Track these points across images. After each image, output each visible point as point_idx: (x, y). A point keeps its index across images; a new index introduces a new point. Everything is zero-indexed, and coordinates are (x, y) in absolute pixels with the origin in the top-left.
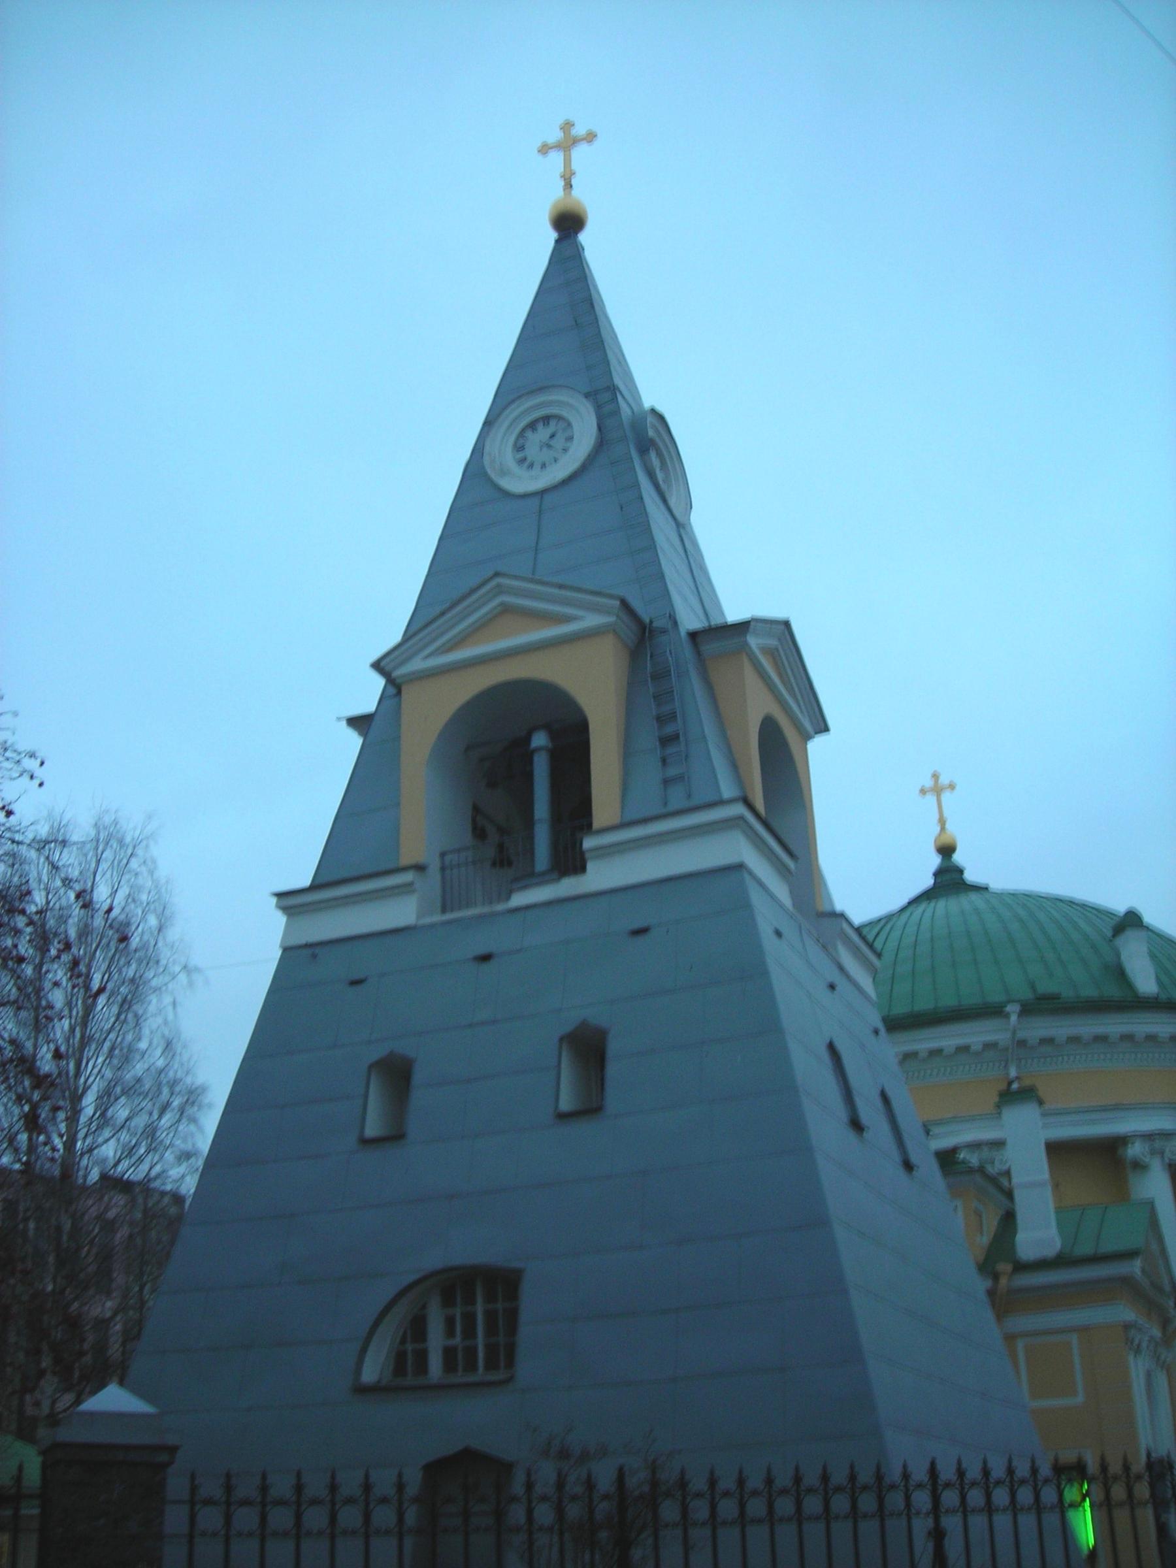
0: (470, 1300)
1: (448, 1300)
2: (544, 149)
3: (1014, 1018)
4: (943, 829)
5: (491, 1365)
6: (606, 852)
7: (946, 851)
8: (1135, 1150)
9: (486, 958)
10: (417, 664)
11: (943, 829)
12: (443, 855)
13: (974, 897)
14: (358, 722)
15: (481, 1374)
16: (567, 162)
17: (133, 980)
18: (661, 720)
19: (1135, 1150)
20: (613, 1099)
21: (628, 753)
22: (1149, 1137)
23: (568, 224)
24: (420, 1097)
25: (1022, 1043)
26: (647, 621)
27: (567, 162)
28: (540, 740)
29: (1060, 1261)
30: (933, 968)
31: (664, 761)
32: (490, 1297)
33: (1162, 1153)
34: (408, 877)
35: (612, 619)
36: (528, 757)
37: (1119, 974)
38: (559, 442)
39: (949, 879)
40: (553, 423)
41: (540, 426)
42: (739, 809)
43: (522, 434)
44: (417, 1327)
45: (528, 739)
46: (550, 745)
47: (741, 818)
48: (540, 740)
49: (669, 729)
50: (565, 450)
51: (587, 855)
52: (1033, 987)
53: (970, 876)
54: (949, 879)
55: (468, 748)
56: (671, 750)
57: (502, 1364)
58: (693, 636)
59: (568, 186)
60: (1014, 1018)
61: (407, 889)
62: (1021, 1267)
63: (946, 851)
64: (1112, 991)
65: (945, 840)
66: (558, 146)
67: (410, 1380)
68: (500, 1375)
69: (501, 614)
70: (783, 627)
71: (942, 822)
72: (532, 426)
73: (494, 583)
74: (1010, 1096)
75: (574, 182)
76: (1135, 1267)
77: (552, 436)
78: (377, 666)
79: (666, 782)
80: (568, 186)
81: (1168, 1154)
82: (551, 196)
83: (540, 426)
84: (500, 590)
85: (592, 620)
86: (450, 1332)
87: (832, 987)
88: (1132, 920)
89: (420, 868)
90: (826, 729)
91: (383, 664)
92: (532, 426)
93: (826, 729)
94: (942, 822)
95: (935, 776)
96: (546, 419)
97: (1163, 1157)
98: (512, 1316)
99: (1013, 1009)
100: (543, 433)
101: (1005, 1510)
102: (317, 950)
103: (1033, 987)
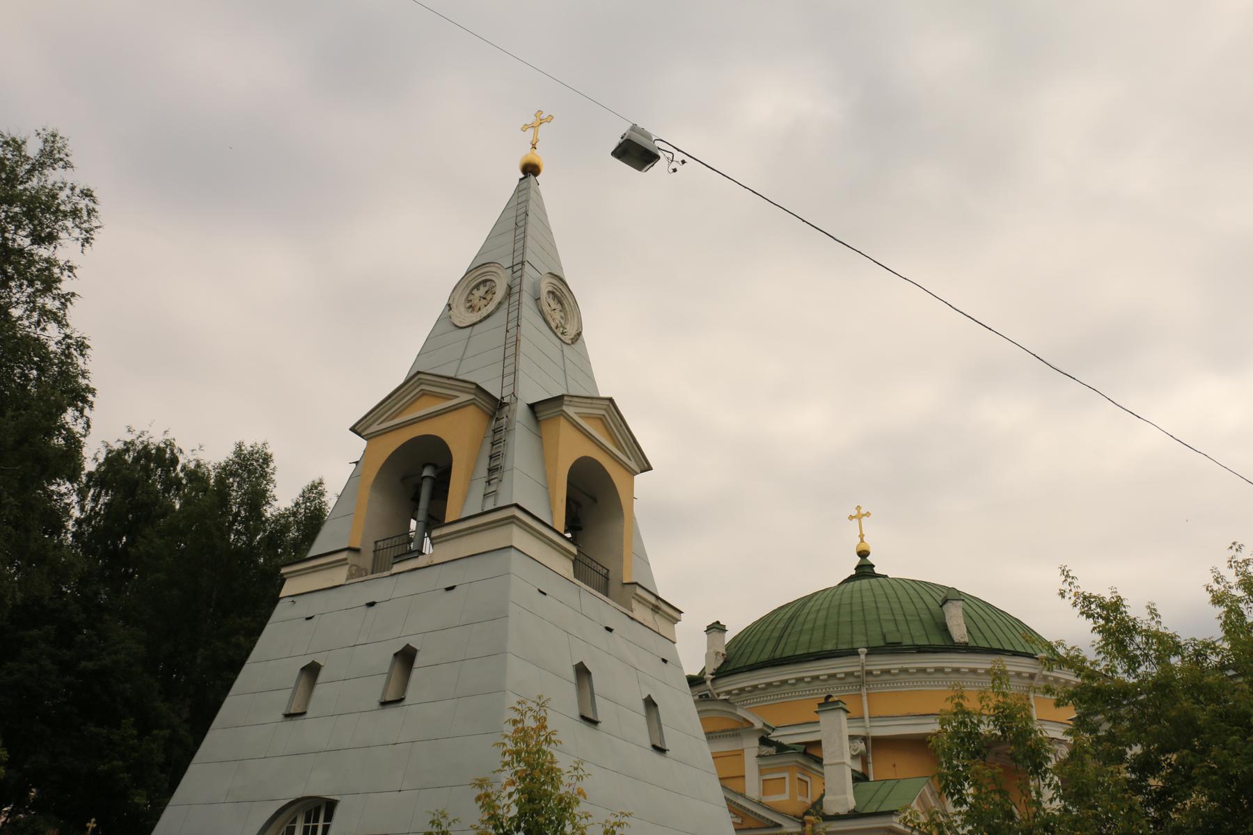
0: (316, 820)
3: (863, 657)
4: (862, 541)
7: (863, 554)
9: (371, 604)
11: (862, 541)
12: (376, 542)
16: (536, 134)
17: (1148, 637)
20: (410, 696)
21: (471, 480)
23: (531, 170)
24: (320, 690)
25: (869, 673)
27: (536, 134)
29: (854, 815)
30: (825, 625)
31: (489, 482)
35: (472, 397)
37: (944, 629)
39: (865, 570)
52: (884, 637)
53: (877, 570)
54: (865, 570)
55: (403, 479)
60: (863, 657)
62: (827, 818)
63: (863, 554)
64: (937, 640)
65: (863, 547)
71: (862, 536)
72: (477, 287)
74: (828, 704)
82: (523, 153)
83: (482, 287)
85: (464, 397)
92: (477, 287)
94: (862, 536)
95: (858, 508)
96: (485, 282)
99: (863, 650)
100: (483, 290)
103: (884, 637)
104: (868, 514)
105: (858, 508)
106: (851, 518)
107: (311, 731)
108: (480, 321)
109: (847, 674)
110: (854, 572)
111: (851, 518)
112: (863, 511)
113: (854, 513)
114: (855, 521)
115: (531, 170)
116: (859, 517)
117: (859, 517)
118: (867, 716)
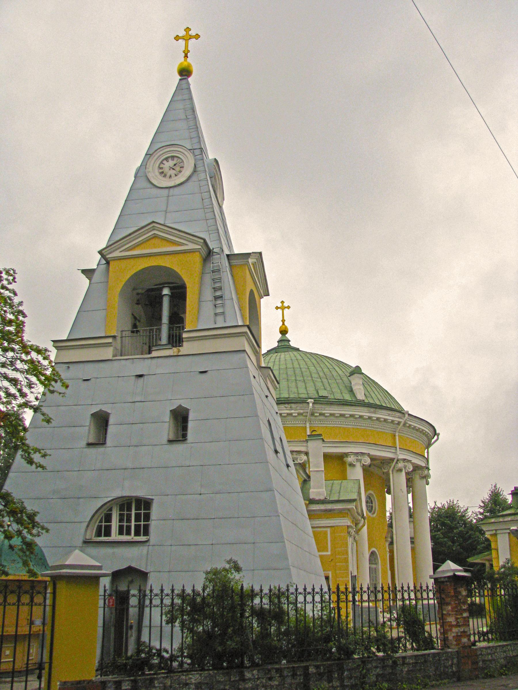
0: (129, 509)
1: (121, 508)
2: (177, 38)
4: (283, 324)
5: (137, 533)
6: (191, 339)
8: (351, 459)
9: (141, 376)
10: (117, 254)
11: (283, 324)
13: (292, 354)
14: (88, 273)
15: (132, 537)
16: (187, 46)
18: (215, 289)
19: (351, 459)
22: (357, 454)
23: (185, 73)
26: (212, 249)
27: (187, 46)
28: (166, 291)
32: (138, 508)
33: (360, 461)
34: (110, 340)
35: (200, 247)
36: (161, 297)
38: (178, 169)
40: (176, 159)
41: (170, 160)
42: (246, 330)
43: (162, 163)
44: (108, 518)
45: (161, 289)
46: (170, 294)
47: (246, 333)
48: (166, 291)
49: (218, 293)
50: (180, 172)
51: (184, 340)
53: (292, 344)
56: (219, 302)
57: (164, 339)
58: (228, 256)
59: (186, 56)
61: (108, 345)
66: (183, 38)
67: (103, 539)
68: (142, 538)
69: (153, 238)
70: (259, 255)
71: (283, 321)
73: (152, 225)
75: (189, 55)
76: (352, 506)
77: (175, 165)
78: (100, 252)
79: (216, 314)
80: (186, 56)
81: (363, 462)
83: (170, 160)
84: (154, 229)
85: (191, 246)
86: (121, 520)
87: (267, 397)
88: (357, 370)
89: (114, 337)
90: (269, 295)
91: (103, 252)
92: (167, 159)
93: (269, 295)
94: (283, 321)
96: (173, 157)
97: (361, 462)
98: (147, 517)
100: (171, 163)
101: (407, 599)
102: (70, 365)
104: (288, 307)
105: (282, 302)
106: (277, 308)
107: (111, 453)
108: (175, 186)
109: (299, 414)
110: (276, 345)
111: (277, 308)
112: (286, 305)
113: (279, 305)
114: (280, 311)
115: (185, 73)
116: (283, 308)
117: (283, 308)
118: (398, 447)
